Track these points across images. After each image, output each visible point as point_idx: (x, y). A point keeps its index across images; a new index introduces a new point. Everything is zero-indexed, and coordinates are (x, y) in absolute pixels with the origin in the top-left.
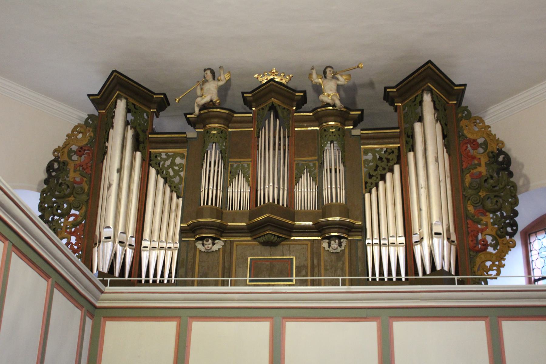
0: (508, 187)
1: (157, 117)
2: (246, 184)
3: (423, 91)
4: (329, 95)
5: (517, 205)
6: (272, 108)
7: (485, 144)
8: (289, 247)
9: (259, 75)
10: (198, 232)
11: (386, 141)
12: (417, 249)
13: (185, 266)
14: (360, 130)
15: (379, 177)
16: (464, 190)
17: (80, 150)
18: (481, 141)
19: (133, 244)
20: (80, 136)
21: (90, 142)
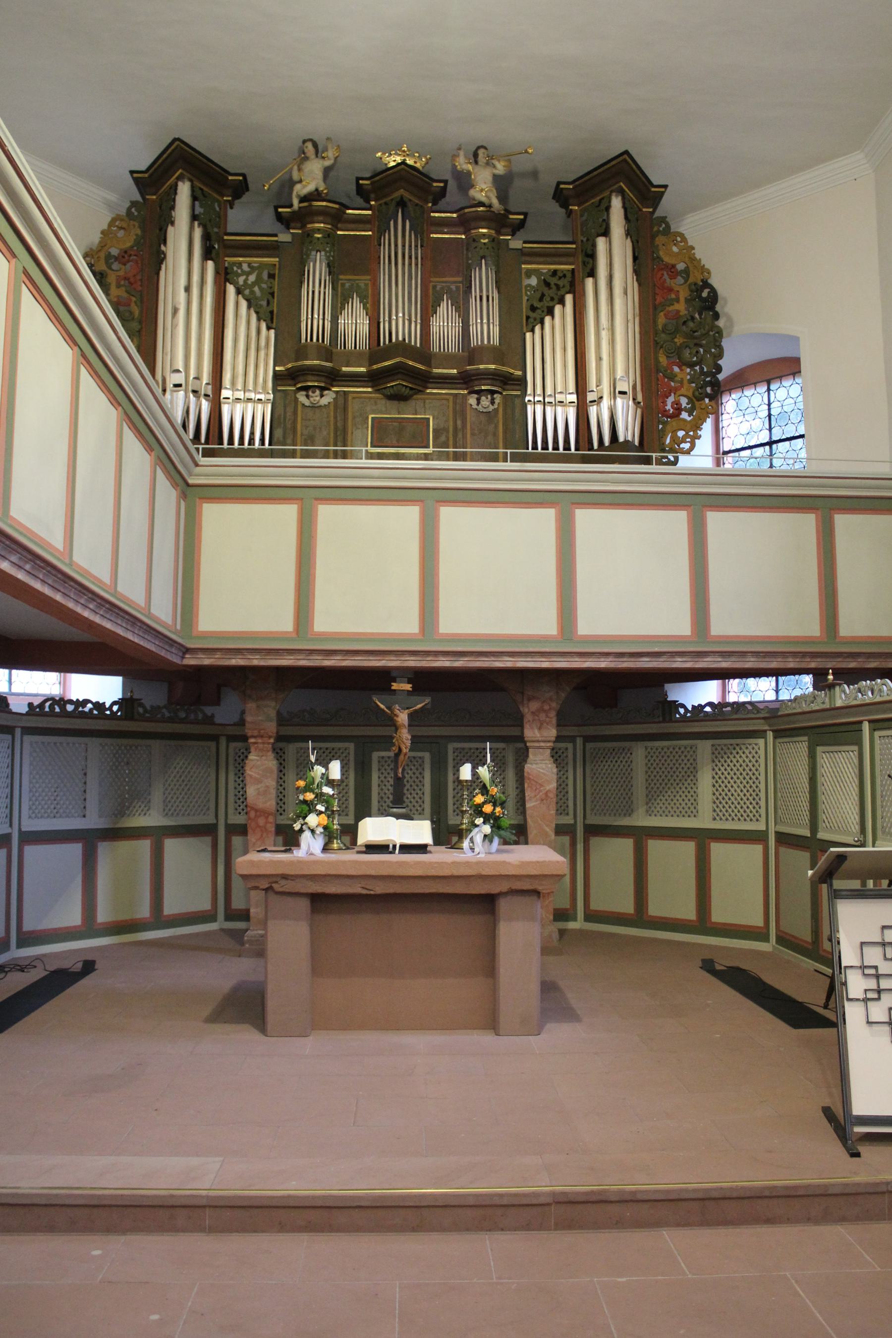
0: (711, 333)
1: (231, 208)
2: (363, 313)
3: (611, 192)
4: (482, 190)
5: (721, 359)
6: (402, 203)
7: (686, 272)
8: (424, 402)
9: (384, 153)
10: (301, 378)
11: (556, 259)
12: (593, 411)
13: (282, 426)
14: (522, 242)
15: (546, 310)
16: (657, 334)
17: (124, 254)
18: (681, 266)
19: (210, 392)
20: (121, 233)
21: (137, 243)
